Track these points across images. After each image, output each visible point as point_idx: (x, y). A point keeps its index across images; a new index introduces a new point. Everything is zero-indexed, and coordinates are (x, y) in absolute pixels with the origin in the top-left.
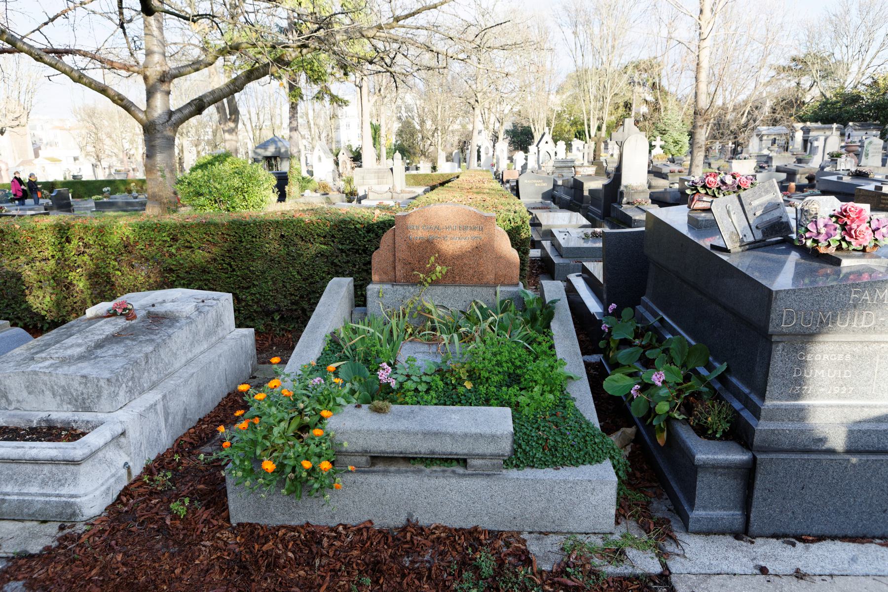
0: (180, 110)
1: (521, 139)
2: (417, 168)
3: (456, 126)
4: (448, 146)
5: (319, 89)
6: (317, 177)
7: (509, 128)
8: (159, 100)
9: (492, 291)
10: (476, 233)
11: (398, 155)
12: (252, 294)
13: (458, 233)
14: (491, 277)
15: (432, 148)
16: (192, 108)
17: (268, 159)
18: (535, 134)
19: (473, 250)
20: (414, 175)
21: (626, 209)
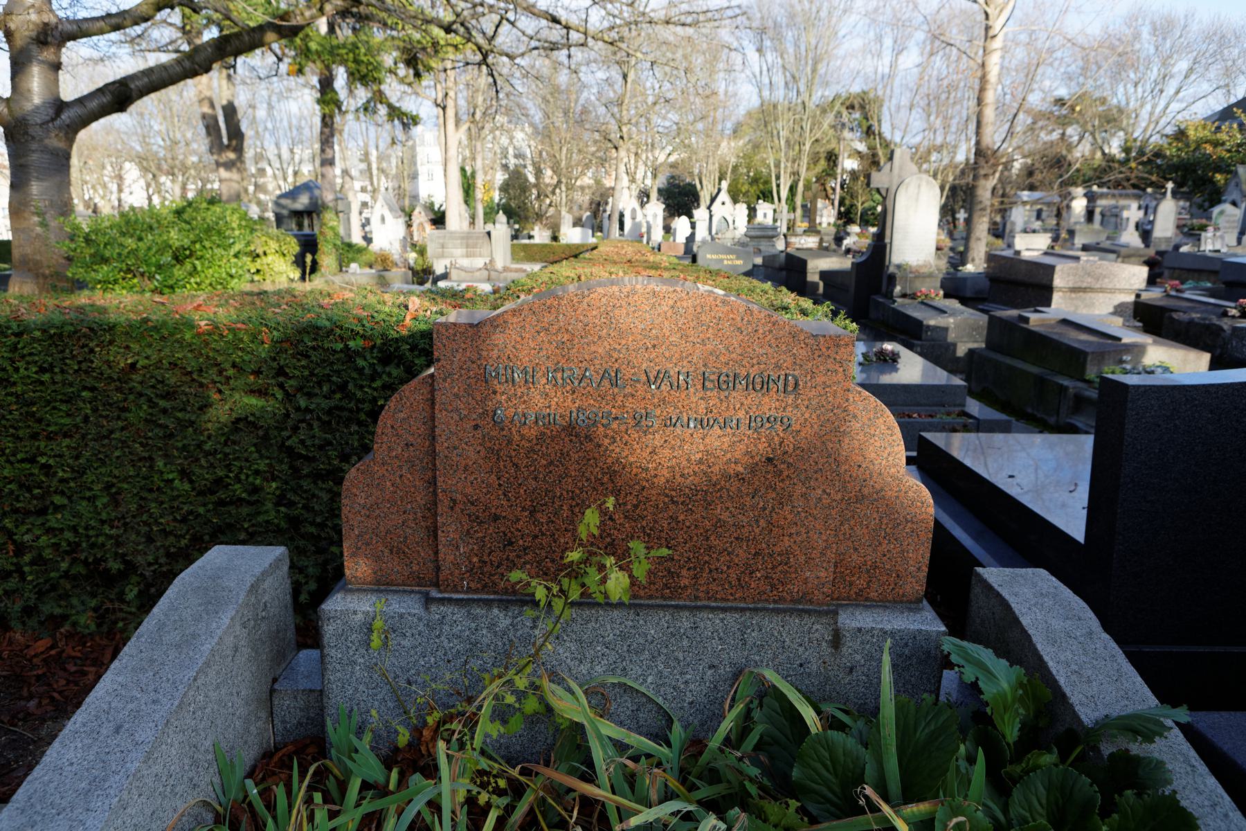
0: (80, 101)
1: (680, 199)
2: (530, 237)
3: (587, 180)
4: (575, 208)
5: (369, 95)
6: (376, 246)
7: (661, 186)
8: (36, 81)
9: (820, 629)
10: (769, 404)
11: (502, 217)
12: (50, 531)
13: (696, 401)
14: (819, 575)
15: (551, 211)
16: (105, 99)
17: (298, 215)
18: (702, 194)
19: (753, 469)
20: (526, 245)
21: (903, 305)
